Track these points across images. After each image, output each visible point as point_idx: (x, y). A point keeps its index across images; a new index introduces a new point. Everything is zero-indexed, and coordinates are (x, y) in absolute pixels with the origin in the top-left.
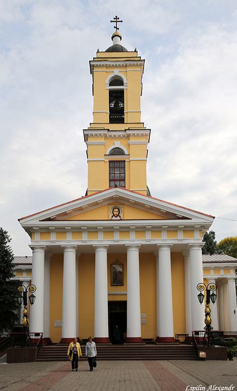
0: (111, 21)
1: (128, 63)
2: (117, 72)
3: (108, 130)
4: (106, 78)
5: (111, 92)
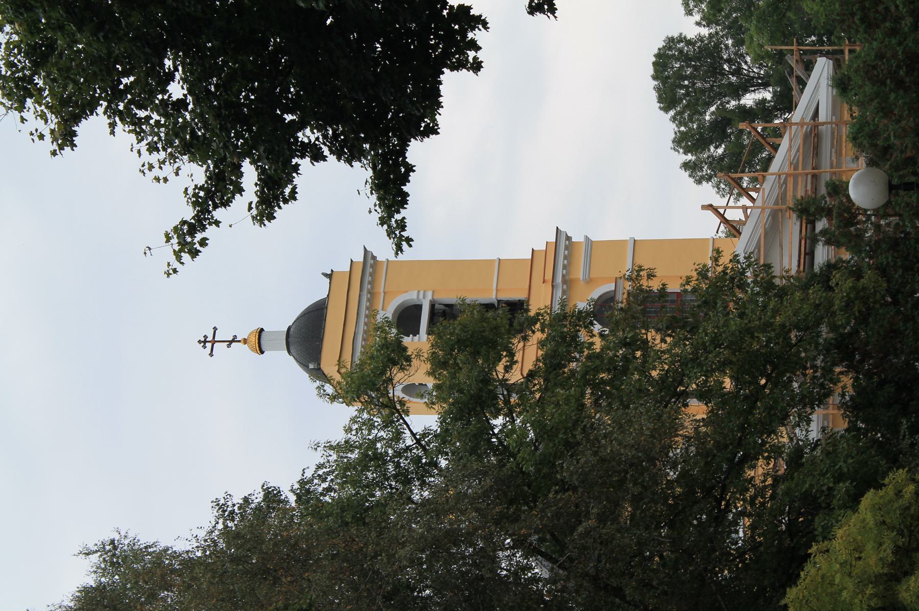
0: (211, 355)
1: (367, 286)
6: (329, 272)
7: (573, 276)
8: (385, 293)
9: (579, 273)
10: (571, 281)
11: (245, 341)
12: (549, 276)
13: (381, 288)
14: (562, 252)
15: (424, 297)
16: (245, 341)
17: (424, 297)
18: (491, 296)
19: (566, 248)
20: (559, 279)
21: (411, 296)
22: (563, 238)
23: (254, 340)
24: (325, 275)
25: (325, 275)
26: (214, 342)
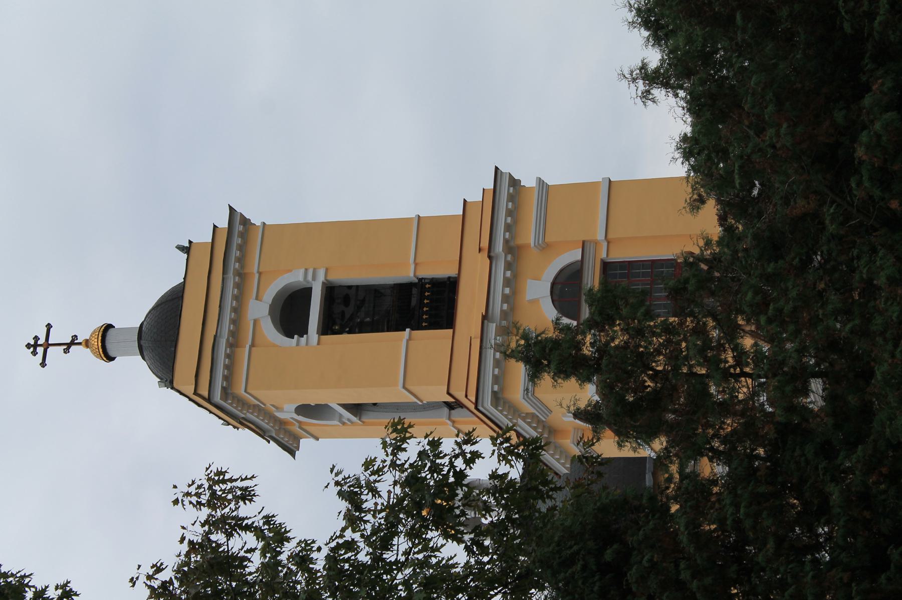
0: (43, 364)
1: (233, 265)
2: (259, 310)
3: (485, 318)
4: (274, 346)
5: (328, 327)
6: (187, 245)
7: (520, 241)
8: (260, 274)
9: (529, 236)
10: (519, 248)
11: (87, 343)
12: (485, 244)
13: (253, 266)
14: (504, 204)
15: (314, 278)
16: (87, 343)
17: (314, 278)
18: (407, 274)
19: (511, 198)
20: (499, 247)
21: (295, 277)
22: (505, 182)
23: (96, 343)
24: (181, 248)
25: (181, 248)
26: (47, 345)
